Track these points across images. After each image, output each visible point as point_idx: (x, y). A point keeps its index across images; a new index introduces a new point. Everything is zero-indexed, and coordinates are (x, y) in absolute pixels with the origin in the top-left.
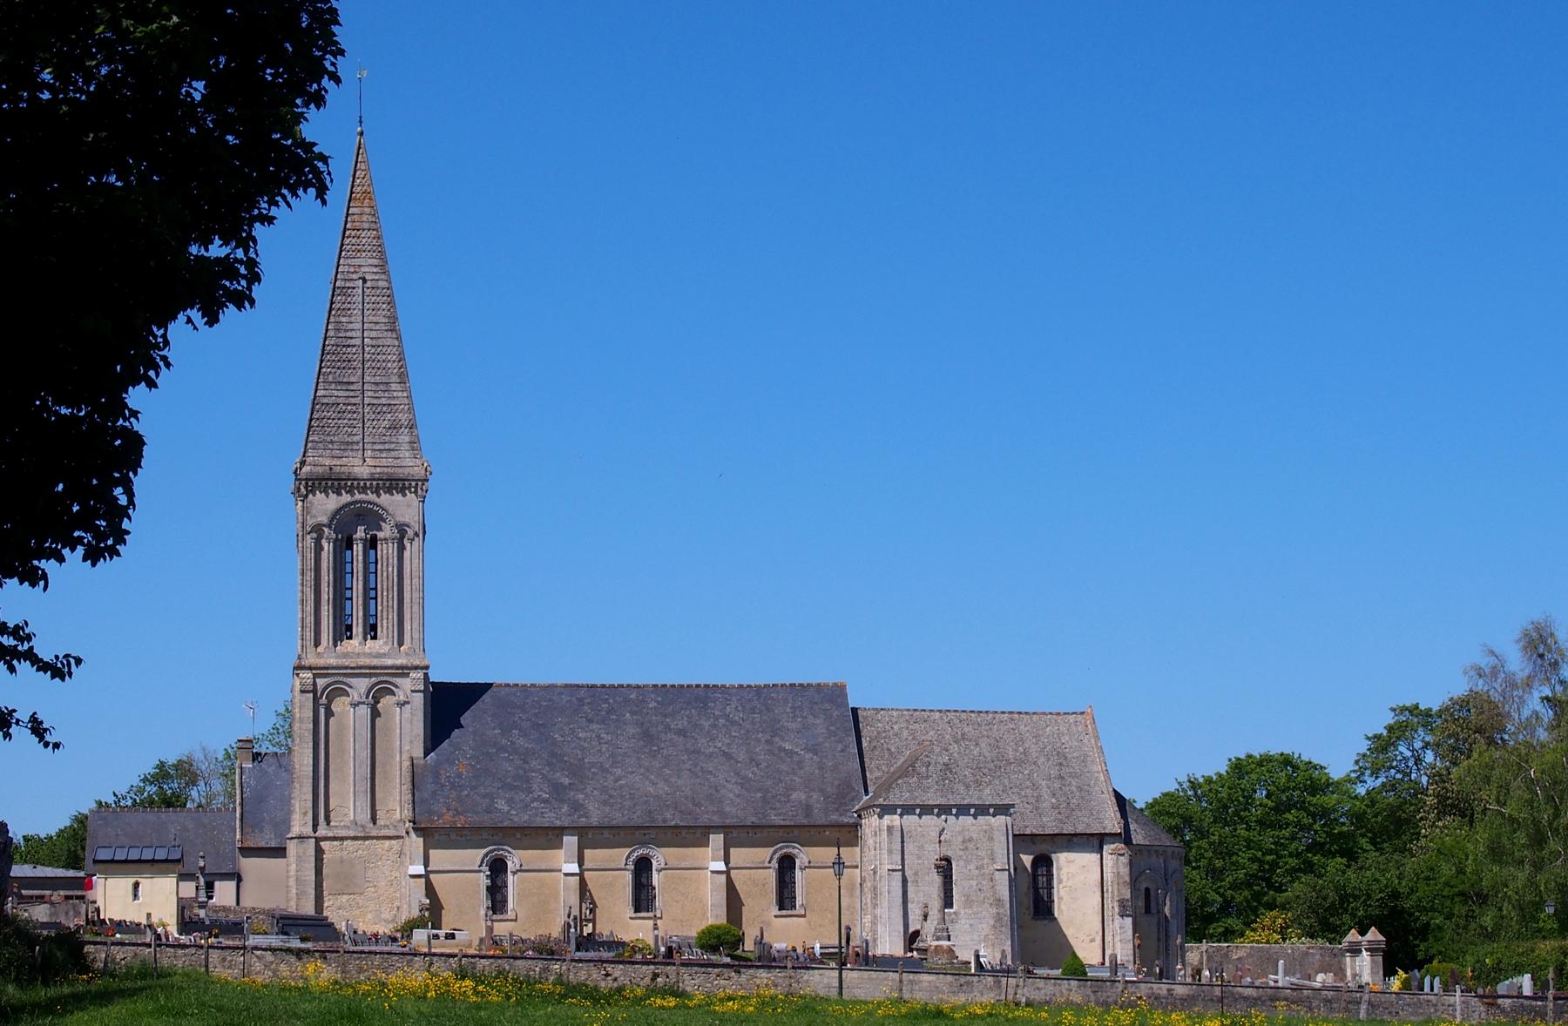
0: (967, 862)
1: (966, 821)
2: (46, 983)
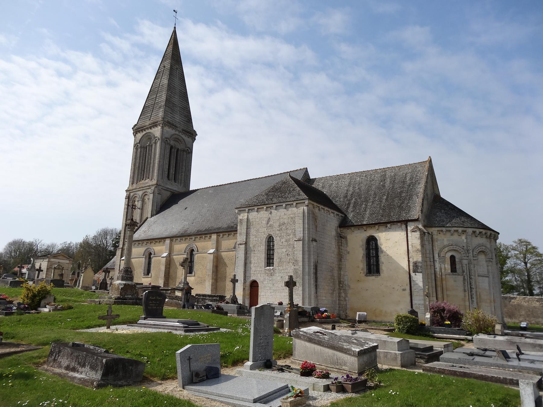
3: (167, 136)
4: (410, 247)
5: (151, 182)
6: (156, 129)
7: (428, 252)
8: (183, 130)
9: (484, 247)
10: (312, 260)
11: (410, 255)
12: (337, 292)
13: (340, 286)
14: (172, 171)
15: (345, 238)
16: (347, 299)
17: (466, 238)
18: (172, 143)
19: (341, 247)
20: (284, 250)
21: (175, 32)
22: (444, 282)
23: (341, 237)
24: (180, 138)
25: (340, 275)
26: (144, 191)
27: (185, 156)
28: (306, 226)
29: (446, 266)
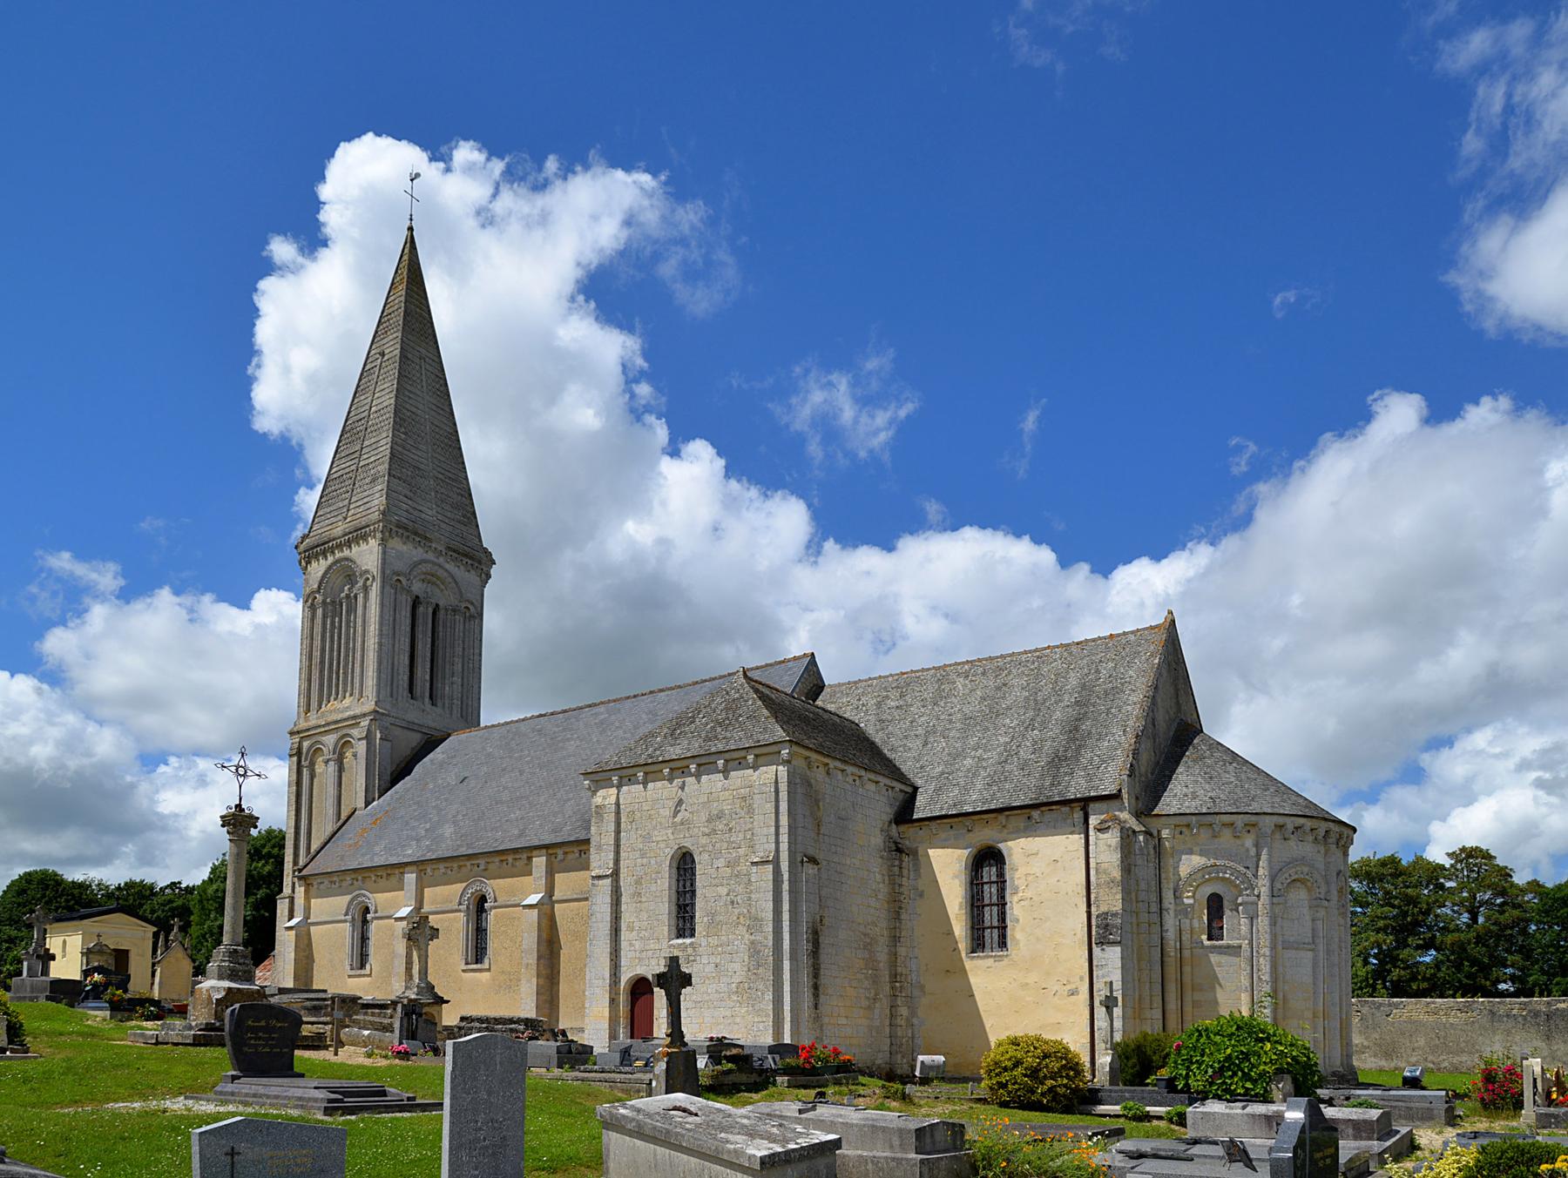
0: (716, 855)
1: (712, 782)
2: (572, 1068)
3: (399, 566)
4: (1092, 872)
5: (358, 702)
6: (364, 546)
7: (1143, 886)
8: (449, 548)
9: (1306, 869)
10: (804, 918)
11: (1093, 896)
12: (886, 1002)
13: (896, 985)
14: (423, 673)
15: (913, 853)
16: (915, 1021)
17: (1257, 845)
18: (417, 587)
19: (898, 881)
20: (723, 891)
21: (411, 242)
22: (1187, 969)
23: (899, 850)
24: (440, 572)
25: (894, 955)
26: (340, 734)
27: (459, 627)
28: (784, 820)
29: (1196, 924)
